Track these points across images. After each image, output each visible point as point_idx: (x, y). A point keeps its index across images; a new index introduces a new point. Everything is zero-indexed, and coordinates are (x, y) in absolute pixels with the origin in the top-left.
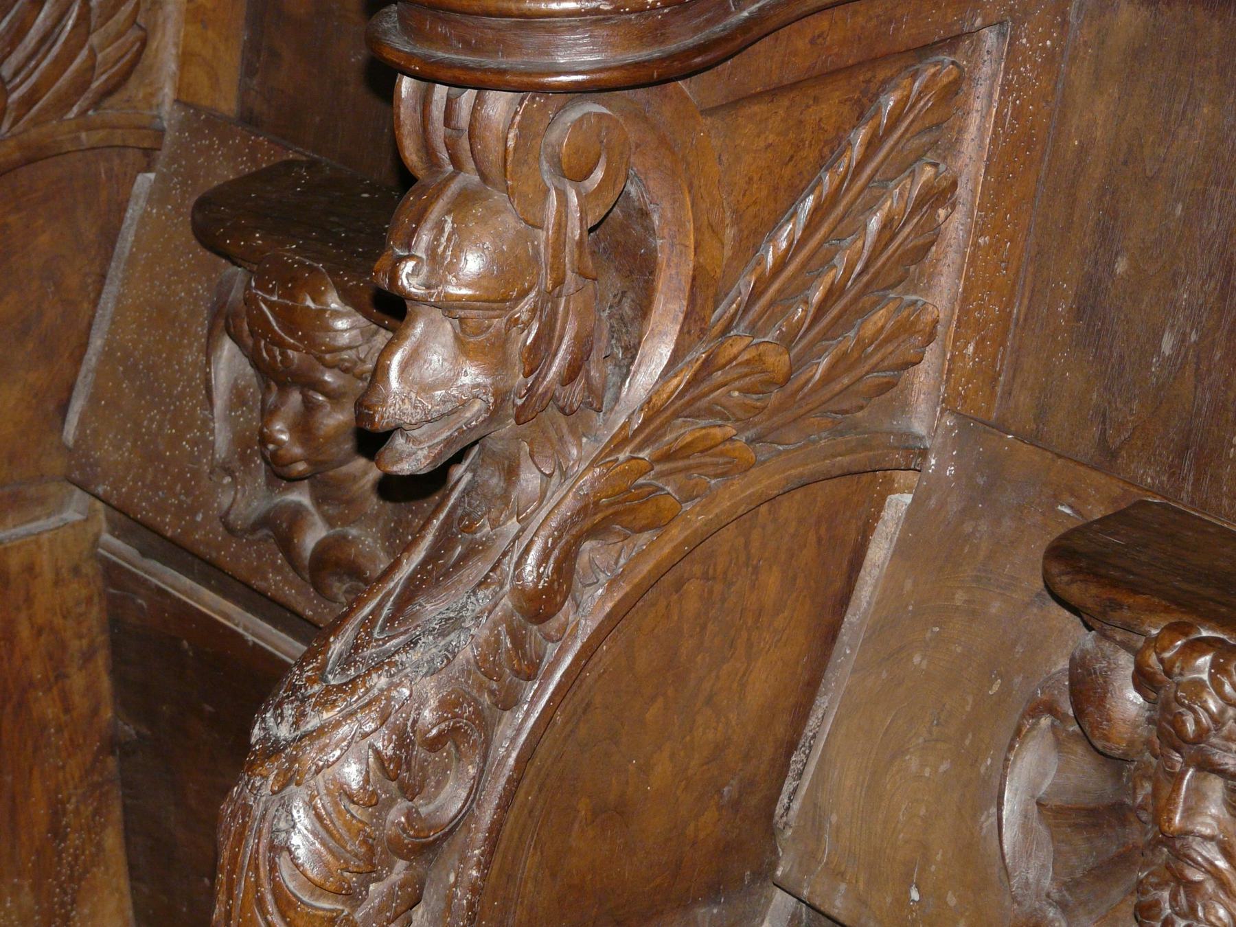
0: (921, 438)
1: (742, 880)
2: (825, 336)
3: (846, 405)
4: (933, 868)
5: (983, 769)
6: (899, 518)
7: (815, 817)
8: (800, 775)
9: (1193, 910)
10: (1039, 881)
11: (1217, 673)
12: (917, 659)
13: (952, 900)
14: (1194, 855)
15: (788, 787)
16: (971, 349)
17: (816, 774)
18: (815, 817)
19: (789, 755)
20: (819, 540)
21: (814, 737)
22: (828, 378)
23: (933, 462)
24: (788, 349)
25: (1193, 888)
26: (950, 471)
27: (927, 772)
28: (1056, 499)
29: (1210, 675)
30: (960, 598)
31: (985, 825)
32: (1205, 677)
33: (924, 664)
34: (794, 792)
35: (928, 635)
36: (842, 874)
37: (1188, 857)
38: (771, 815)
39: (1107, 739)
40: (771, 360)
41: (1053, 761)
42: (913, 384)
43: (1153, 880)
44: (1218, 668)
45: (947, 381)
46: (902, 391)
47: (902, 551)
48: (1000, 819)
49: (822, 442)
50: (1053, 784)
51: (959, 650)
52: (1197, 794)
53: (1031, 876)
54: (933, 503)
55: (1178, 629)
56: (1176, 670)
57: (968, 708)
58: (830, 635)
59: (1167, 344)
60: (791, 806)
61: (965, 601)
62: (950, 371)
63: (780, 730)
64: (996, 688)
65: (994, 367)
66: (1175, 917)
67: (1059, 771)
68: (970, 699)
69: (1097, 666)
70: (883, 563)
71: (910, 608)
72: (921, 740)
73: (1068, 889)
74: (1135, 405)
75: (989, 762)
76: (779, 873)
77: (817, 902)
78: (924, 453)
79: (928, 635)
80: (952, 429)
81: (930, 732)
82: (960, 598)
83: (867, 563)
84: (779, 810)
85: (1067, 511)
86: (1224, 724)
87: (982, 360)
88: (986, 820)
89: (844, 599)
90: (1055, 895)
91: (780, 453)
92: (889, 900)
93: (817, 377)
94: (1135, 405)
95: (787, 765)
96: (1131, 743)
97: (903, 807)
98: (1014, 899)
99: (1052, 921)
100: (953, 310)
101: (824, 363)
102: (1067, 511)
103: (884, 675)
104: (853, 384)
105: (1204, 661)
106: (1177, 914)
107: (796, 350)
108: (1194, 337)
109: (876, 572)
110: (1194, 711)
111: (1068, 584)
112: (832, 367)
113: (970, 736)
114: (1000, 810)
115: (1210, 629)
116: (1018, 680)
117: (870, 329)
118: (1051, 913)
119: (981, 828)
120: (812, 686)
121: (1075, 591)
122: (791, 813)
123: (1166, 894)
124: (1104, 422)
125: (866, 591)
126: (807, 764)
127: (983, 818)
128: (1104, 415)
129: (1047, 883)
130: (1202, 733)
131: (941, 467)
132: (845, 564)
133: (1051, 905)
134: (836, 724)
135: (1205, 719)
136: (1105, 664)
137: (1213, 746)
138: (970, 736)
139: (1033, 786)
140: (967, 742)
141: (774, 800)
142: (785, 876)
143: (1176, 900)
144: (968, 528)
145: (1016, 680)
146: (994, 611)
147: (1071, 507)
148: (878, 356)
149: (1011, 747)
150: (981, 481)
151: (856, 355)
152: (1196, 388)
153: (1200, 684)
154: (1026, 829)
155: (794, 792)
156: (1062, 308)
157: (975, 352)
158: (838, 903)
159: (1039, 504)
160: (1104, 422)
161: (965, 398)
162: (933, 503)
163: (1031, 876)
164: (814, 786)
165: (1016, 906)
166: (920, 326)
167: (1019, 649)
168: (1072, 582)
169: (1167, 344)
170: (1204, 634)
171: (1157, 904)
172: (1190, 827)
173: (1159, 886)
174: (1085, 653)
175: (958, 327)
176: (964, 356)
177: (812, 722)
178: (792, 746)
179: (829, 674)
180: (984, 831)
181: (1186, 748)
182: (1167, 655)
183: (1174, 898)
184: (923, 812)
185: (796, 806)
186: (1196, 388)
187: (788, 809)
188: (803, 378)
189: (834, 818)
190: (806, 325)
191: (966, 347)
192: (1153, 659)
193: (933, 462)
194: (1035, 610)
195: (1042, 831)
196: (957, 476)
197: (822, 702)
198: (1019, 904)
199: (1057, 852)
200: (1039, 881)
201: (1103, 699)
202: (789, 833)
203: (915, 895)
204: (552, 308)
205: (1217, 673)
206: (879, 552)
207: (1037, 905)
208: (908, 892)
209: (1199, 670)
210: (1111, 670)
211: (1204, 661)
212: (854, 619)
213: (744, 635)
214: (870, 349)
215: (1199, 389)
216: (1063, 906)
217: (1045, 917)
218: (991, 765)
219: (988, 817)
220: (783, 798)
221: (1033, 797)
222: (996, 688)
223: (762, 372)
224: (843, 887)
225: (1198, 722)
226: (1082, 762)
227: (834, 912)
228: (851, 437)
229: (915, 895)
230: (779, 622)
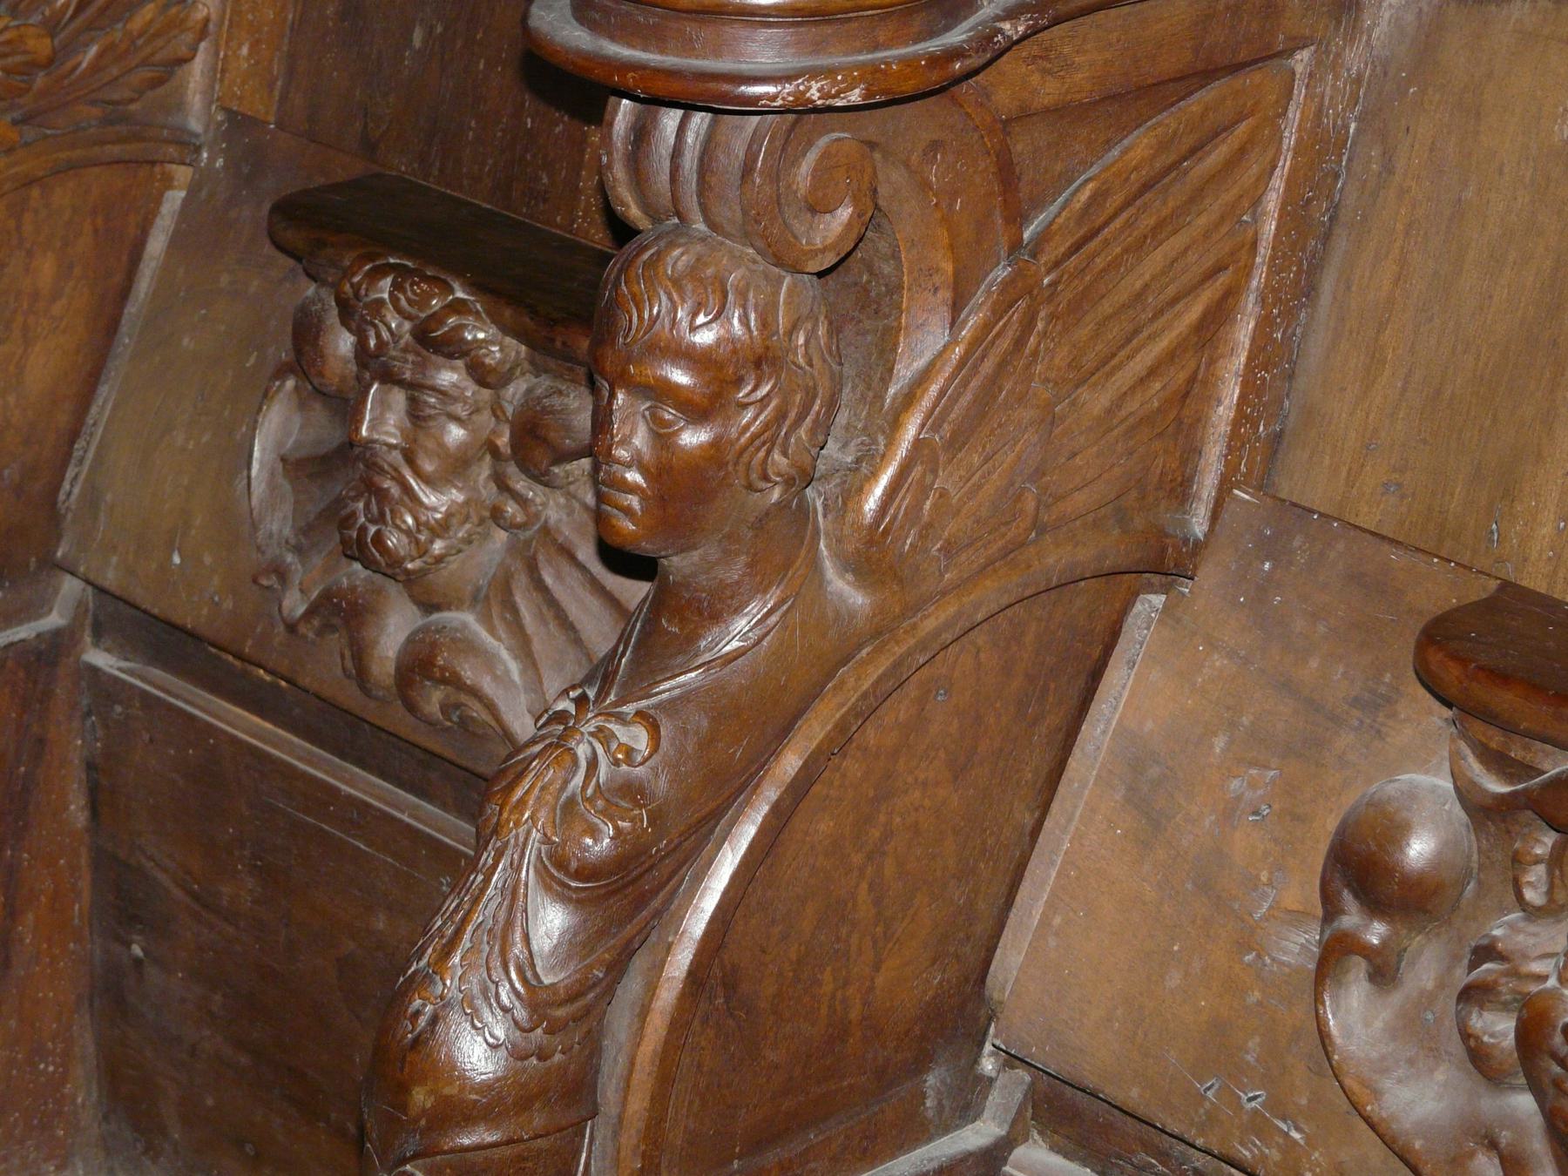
0: (197, 136)
1: (28, 566)
2: (90, 27)
3: (116, 96)
4: (193, 532)
7: (92, 498)
8: (81, 461)
9: (382, 514)
12: (186, 341)
13: (208, 560)
14: (381, 462)
15: (70, 474)
16: (245, 51)
17: (94, 460)
18: (92, 498)
19: (73, 442)
20: (96, 231)
21: (94, 424)
22: (96, 67)
24: (52, 36)
25: (382, 495)
26: (220, 163)
29: (391, 293)
30: (225, 280)
32: (386, 296)
34: (76, 478)
36: (115, 548)
37: (375, 464)
38: (54, 504)
40: (31, 43)
41: (297, 420)
43: (352, 494)
44: (396, 286)
45: (222, 80)
47: (177, 242)
49: (92, 130)
51: (223, 328)
52: (383, 404)
53: (275, 528)
54: (203, 194)
56: (363, 292)
58: (112, 328)
59: (417, 38)
60: (71, 491)
62: (223, 71)
63: (63, 419)
64: (252, 360)
67: (302, 427)
68: (230, 373)
73: (304, 534)
76: (59, 554)
77: (92, 577)
78: (198, 150)
82: (225, 280)
83: (146, 256)
84: (62, 497)
86: (401, 337)
87: (257, 63)
89: (125, 292)
90: (293, 541)
91: (46, 137)
92: (154, 566)
93: (84, 65)
95: (69, 455)
98: (259, 548)
100: (224, 12)
101: (93, 50)
104: (122, 75)
105: (387, 283)
107: (62, 35)
108: (439, 29)
109: (153, 264)
110: (375, 326)
112: (100, 55)
114: (249, 469)
117: (137, 23)
118: (290, 558)
120: (93, 378)
121: (291, 236)
122: (73, 498)
123: (361, 505)
125: (144, 284)
126: (87, 449)
129: (287, 532)
131: (212, 159)
132: (125, 258)
134: (115, 408)
135: (385, 335)
137: (394, 358)
139: (280, 444)
141: (57, 488)
142: (64, 556)
144: (233, 214)
148: (148, 50)
149: (260, 409)
150: (246, 170)
151: (123, 47)
153: (381, 302)
154: (272, 486)
155: (76, 478)
156: (330, 11)
157: (250, 54)
161: (240, 98)
162: (203, 194)
163: (275, 528)
164: (92, 469)
166: (190, 24)
167: (273, 323)
169: (417, 38)
171: (353, 515)
173: (356, 499)
175: (230, 26)
176: (238, 57)
177: (94, 410)
178: (74, 435)
179: (110, 365)
183: (367, 506)
184: (186, 482)
185: (76, 491)
187: (69, 494)
188: (69, 65)
189: (109, 497)
190: (70, 12)
191: (240, 47)
192: (347, 288)
195: (287, 487)
196: (225, 167)
197: (103, 390)
198: (263, 553)
199: (296, 502)
201: (317, 337)
202: (70, 516)
203: (177, 559)
204: (375, 562)
206: (157, 245)
209: (382, 291)
211: (387, 283)
212: (133, 310)
213: (20, 319)
214: (140, 42)
216: (298, 550)
220: (66, 486)
222: (252, 360)
223: (25, 52)
224: (114, 559)
225: (378, 336)
226: (319, 413)
228: (122, 129)
229: (177, 559)
230: (57, 309)
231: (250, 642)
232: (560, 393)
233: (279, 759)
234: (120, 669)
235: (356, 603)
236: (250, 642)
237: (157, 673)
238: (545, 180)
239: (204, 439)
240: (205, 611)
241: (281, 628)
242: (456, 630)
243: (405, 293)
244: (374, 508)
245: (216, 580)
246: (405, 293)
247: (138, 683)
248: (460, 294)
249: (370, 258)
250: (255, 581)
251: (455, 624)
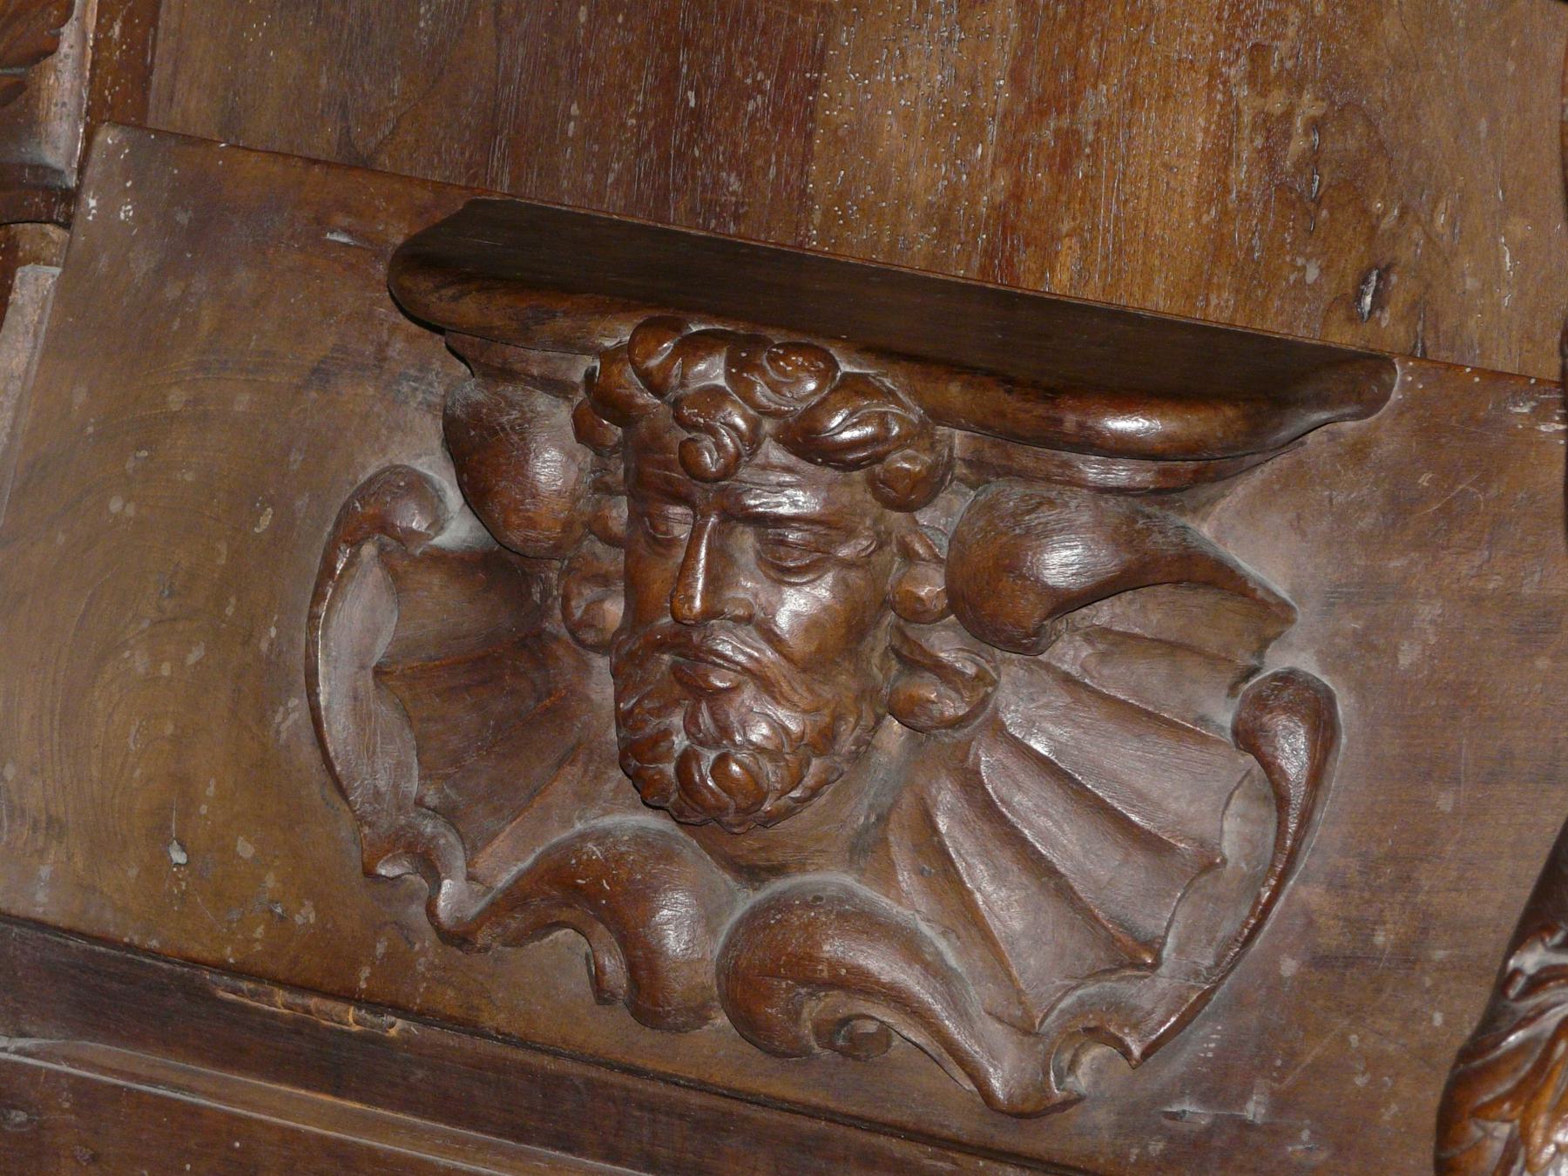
4: (204, 809)
5: (264, 646)
6: (45, 299)
10: (396, 786)
11: (740, 372)
12: (115, 505)
13: (245, 849)
16: (117, 29)
23: (93, 203)
26: (126, 212)
27: (166, 669)
28: (322, 222)
31: (283, 727)
33: (130, 510)
35: (130, 465)
39: (531, 523)
42: (39, 90)
46: (27, 100)
48: (314, 709)
50: (396, 641)
55: (652, 329)
56: (674, 381)
57: (222, 561)
61: (187, 402)
64: (266, 521)
65: (144, 59)
66: (698, 748)
68: (223, 548)
69: (504, 419)
70: (27, 372)
71: (90, 430)
72: (145, 625)
74: (397, 84)
75: (273, 632)
79: (130, 465)
80: (118, 148)
81: (160, 609)
82: (176, 399)
85: (344, 239)
87: (130, 47)
88: (284, 719)
92: (133, 873)
94: (397, 84)
96: (568, 525)
97: (133, 730)
99: (434, 837)
102: (344, 239)
103: (61, 539)
106: (701, 743)
111: (455, 299)
113: (233, 600)
114: (312, 693)
115: (701, 322)
116: (301, 503)
119: (278, 733)
123: (677, 720)
124: (345, 118)
127: (278, 718)
128: (344, 106)
130: (729, 471)
131: (108, 208)
133: (425, 816)
136: (515, 414)
138: (233, 600)
140: (229, 611)
143: (697, 724)
144: (172, 291)
145: (299, 503)
146: (239, 408)
147: (347, 231)
150: (183, 218)
152: (499, 40)
154: (361, 717)
158: (41, 897)
159: (292, 237)
160: (345, 118)
163: (383, 784)
165: (366, 830)
167: (296, 457)
168: (462, 295)
170: (694, 330)
172: (719, 607)
173: (664, 710)
174: (474, 409)
180: (284, 736)
181: (698, 492)
182: (653, 363)
183: (691, 722)
186: (499, 40)
191: (111, 27)
193: (93, 203)
194: (313, 394)
195: (386, 713)
198: (371, 825)
200: (396, 786)
205: (740, 372)
207: (402, 820)
208: (165, 855)
210: (529, 422)
215: (506, 43)
216: (449, 814)
217: (421, 834)
218: (278, 636)
219: (287, 714)
221: (363, 667)
222: (266, 521)
227: (38, 912)
229: (179, 857)
231: (365, 972)
232: (1051, 503)
233: (390, 1154)
234: (19, 1052)
235: (632, 881)
236: (365, 972)
237: (96, 1048)
238: (735, 185)
239: (192, 658)
240: (259, 932)
241: (429, 939)
242: (841, 901)
243: (763, 373)
244: (705, 718)
245: (270, 881)
246: (763, 373)
247: (64, 1068)
248: (845, 368)
249: (676, 326)
250: (369, 873)
251: (831, 891)
